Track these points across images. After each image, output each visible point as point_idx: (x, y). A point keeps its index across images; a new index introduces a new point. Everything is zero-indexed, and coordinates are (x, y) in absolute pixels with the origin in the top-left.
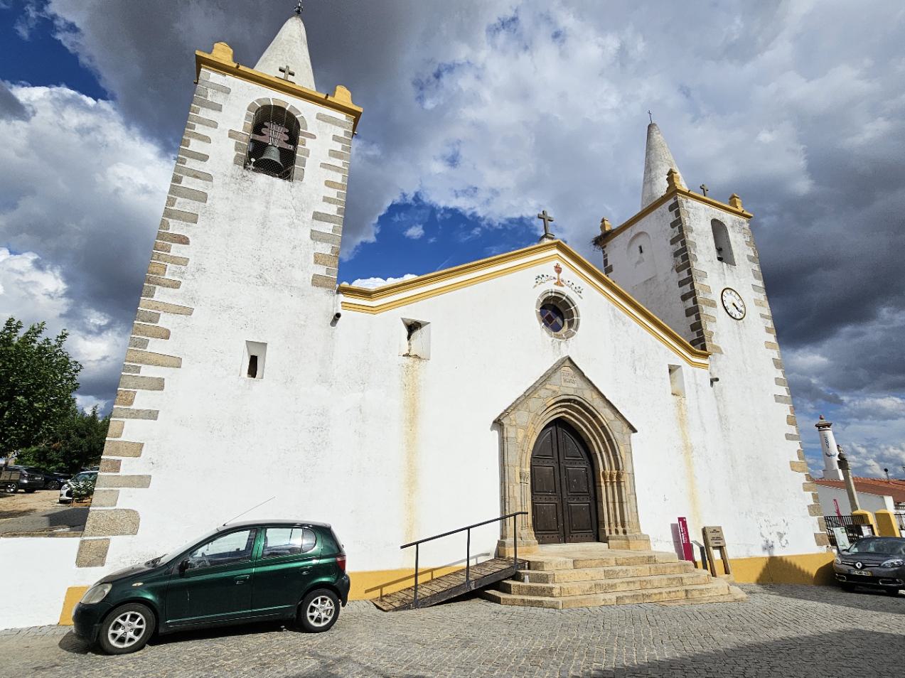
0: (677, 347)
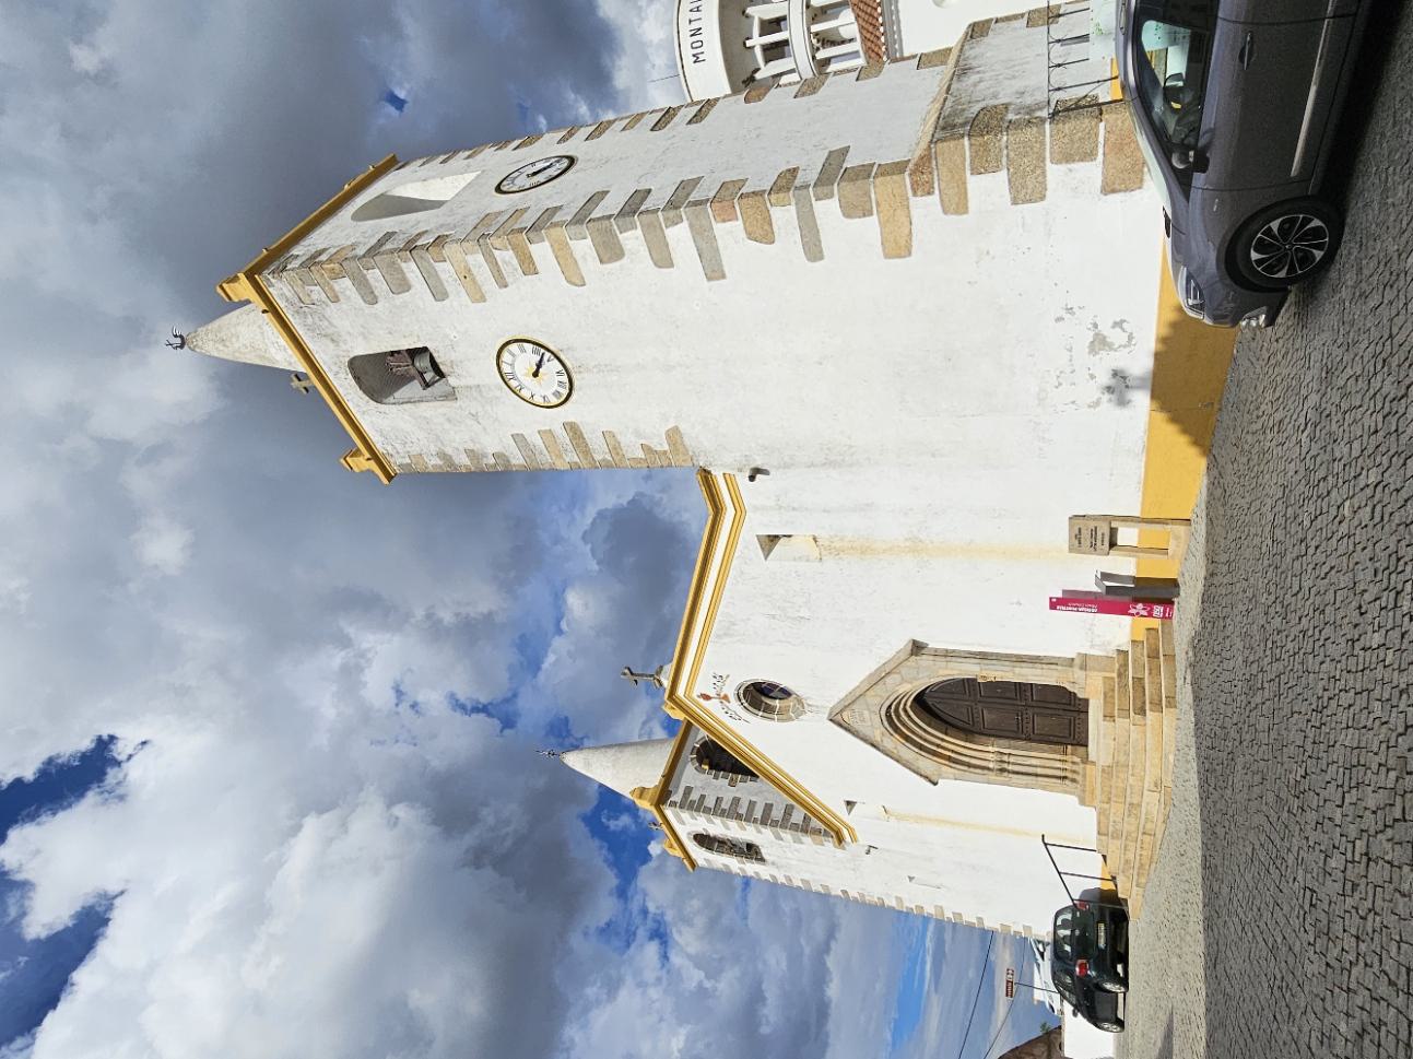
0: (821, 810)
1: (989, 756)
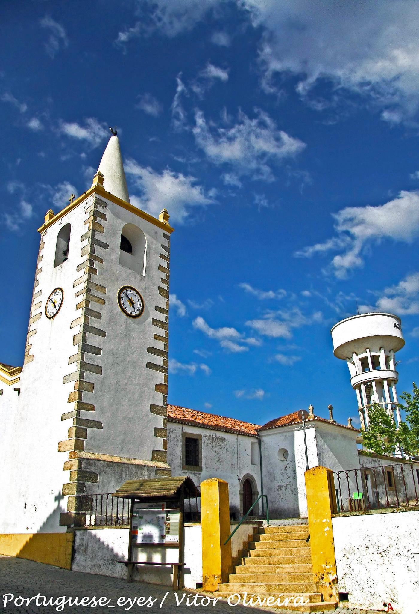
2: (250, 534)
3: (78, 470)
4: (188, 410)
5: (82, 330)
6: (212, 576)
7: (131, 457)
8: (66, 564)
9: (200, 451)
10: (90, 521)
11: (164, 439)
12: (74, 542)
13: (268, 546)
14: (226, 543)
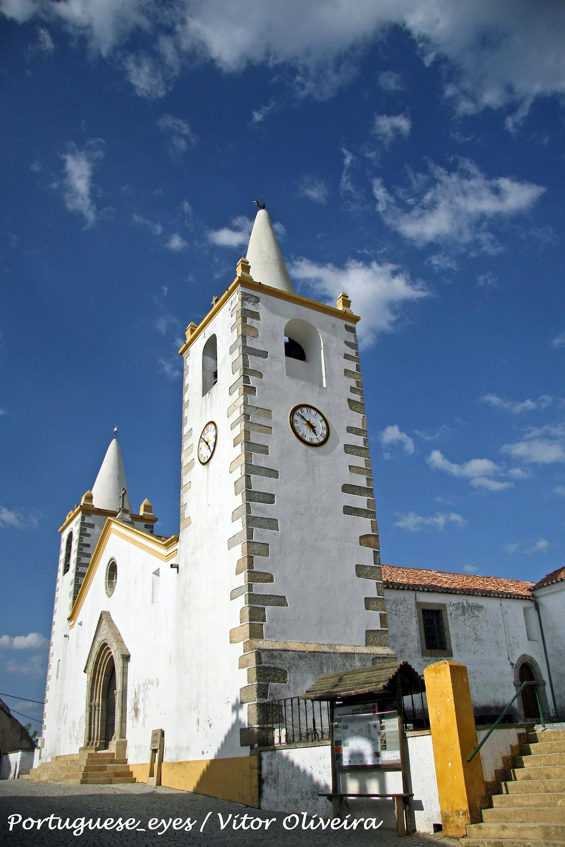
1: (97, 700)
2: (513, 744)
3: (256, 667)
4: (429, 572)
5: (243, 473)
6: (454, 812)
7: (334, 643)
8: (253, 800)
9: (445, 628)
10: (280, 738)
11: (382, 612)
12: (260, 768)
13: (542, 761)
14: (471, 759)
